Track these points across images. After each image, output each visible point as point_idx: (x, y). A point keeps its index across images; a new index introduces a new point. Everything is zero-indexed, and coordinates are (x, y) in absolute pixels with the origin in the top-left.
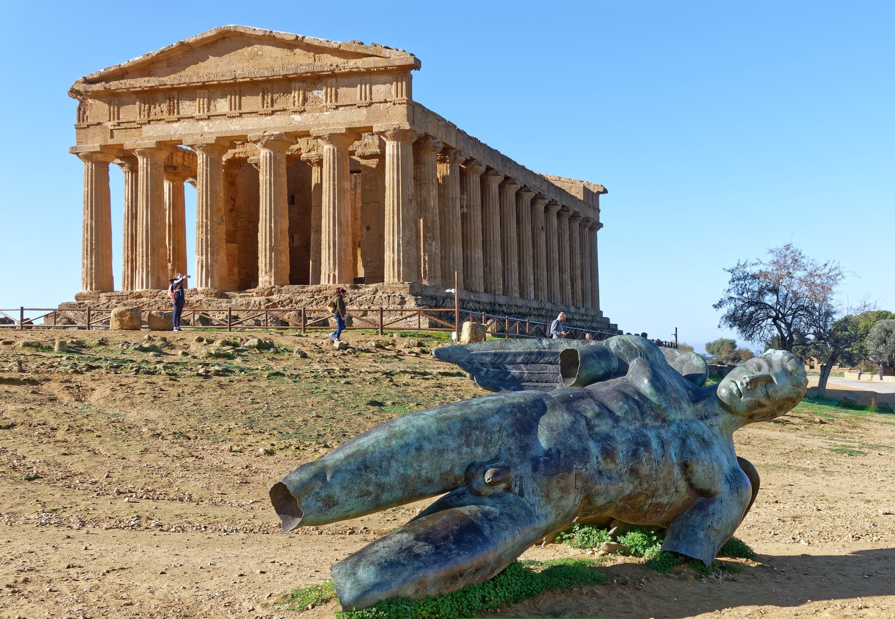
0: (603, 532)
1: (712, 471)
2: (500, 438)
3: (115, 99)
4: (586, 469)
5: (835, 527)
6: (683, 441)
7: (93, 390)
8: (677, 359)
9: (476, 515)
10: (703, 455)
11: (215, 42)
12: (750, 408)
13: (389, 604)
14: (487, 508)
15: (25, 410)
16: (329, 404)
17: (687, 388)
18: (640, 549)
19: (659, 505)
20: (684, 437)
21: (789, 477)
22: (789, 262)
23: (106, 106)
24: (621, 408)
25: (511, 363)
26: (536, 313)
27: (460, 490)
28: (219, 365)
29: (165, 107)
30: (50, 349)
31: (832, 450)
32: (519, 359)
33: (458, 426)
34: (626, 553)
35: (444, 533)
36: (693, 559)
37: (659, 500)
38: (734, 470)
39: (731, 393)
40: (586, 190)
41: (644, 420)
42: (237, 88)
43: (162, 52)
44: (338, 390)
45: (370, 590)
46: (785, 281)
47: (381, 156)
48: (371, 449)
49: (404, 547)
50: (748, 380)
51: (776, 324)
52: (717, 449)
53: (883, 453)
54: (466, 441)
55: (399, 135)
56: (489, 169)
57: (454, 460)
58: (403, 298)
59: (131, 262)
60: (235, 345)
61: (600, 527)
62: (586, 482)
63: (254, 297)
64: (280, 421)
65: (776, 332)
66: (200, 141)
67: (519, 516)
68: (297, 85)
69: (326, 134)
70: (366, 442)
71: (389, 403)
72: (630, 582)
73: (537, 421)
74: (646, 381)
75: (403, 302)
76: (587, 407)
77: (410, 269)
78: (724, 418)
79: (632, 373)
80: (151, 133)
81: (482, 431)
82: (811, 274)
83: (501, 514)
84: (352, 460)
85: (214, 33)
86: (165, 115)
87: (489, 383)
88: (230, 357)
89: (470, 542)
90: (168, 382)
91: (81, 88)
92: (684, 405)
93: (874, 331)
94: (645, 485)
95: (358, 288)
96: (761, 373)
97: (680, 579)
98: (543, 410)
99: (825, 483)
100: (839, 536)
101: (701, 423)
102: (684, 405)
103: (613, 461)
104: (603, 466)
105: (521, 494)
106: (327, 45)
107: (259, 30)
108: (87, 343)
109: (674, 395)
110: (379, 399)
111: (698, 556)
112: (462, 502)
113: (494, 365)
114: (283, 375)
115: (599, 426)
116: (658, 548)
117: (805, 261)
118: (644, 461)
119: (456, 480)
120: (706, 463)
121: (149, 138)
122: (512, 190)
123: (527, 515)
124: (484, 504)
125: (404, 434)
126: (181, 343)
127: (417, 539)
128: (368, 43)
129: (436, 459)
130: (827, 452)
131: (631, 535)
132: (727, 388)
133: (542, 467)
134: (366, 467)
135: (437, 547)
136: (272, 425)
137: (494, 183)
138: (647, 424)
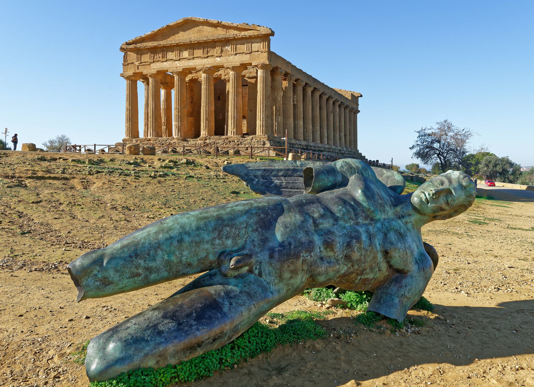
0: (330, 291)
1: (405, 256)
2: (247, 233)
3: (139, 52)
4: (311, 256)
5: (481, 279)
6: (386, 235)
7: (94, 183)
8: (384, 176)
9: (219, 294)
10: (399, 245)
11: (183, 25)
12: (434, 212)
13: (129, 376)
14: (230, 287)
15: (52, 193)
16: (211, 193)
17: (390, 196)
18: (354, 304)
19: (366, 279)
20: (386, 231)
21: (449, 239)
22: (446, 128)
23: (135, 55)
24: (340, 211)
25: (274, 176)
26: (327, 150)
27: (214, 271)
28: (163, 172)
29: (160, 55)
30: (84, 162)
31: (470, 221)
32: (281, 174)
33: (213, 224)
34: (344, 307)
35: (188, 311)
36: (390, 318)
37: (366, 276)
38: (421, 255)
39: (421, 201)
40: (352, 95)
41: (357, 219)
42: (191, 46)
43: (159, 30)
44: (218, 185)
45: (113, 365)
46: (444, 137)
47: (256, 77)
48: (142, 241)
49: (151, 325)
50: (434, 191)
51: (439, 157)
52: (409, 240)
53: (496, 223)
54: (219, 235)
55: (264, 67)
56: (306, 84)
57: (208, 250)
58: (264, 142)
59: (147, 125)
60: (176, 162)
61: (329, 287)
62: (311, 266)
63: (199, 141)
64: (182, 201)
65: (439, 160)
66: (175, 70)
67: (255, 293)
68: (218, 44)
69: (231, 66)
70: (140, 235)
71: (242, 192)
72: (342, 336)
73: (276, 220)
74: (360, 191)
75: (264, 144)
76: (315, 210)
77: (268, 129)
78: (415, 217)
79: (351, 185)
80: (154, 67)
81: (232, 227)
82: (456, 134)
83: (241, 292)
84: (126, 250)
85: (182, 21)
86: (161, 59)
87: (258, 188)
88: (171, 168)
89: (210, 318)
90: (134, 180)
91: (125, 47)
92: (387, 208)
93: (483, 162)
94: (356, 267)
95: (245, 137)
96: (443, 187)
97: (380, 333)
98: (281, 212)
99: (469, 243)
100: (485, 287)
101: (399, 221)
102: (387, 208)
103: (332, 250)
104: (324, 254)
105: (260, 275)
106: (232, 25)
107: (201, 18)
108: (105, 160)
109: (380, 201)
110: (237, 190)
111: (393, 317)
112: (212, 281)
113: (263, 177)
114: (193, 177)
115: (322, 224)
116: (366, 304)
117: (453, 128)
118: (355, 250)
119: (211, 263)
120: (401, 251)
121: (154, 69)
122: (317, 94)
123: (263, 292)
124: (228, 284)
125: (170, 229)
126: (150, 161)
127: (165, 317)
128: (250, 24)
129: (193, 249)
130: (467, 222)
131: (349, 293)
132: (418, 197)
133: (276, 255)
134: (137, 255)
135: (180, 324)
136: (177, 203)
137: (309, 91)
138: (359, 222)
